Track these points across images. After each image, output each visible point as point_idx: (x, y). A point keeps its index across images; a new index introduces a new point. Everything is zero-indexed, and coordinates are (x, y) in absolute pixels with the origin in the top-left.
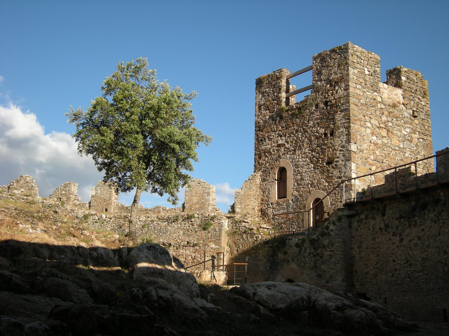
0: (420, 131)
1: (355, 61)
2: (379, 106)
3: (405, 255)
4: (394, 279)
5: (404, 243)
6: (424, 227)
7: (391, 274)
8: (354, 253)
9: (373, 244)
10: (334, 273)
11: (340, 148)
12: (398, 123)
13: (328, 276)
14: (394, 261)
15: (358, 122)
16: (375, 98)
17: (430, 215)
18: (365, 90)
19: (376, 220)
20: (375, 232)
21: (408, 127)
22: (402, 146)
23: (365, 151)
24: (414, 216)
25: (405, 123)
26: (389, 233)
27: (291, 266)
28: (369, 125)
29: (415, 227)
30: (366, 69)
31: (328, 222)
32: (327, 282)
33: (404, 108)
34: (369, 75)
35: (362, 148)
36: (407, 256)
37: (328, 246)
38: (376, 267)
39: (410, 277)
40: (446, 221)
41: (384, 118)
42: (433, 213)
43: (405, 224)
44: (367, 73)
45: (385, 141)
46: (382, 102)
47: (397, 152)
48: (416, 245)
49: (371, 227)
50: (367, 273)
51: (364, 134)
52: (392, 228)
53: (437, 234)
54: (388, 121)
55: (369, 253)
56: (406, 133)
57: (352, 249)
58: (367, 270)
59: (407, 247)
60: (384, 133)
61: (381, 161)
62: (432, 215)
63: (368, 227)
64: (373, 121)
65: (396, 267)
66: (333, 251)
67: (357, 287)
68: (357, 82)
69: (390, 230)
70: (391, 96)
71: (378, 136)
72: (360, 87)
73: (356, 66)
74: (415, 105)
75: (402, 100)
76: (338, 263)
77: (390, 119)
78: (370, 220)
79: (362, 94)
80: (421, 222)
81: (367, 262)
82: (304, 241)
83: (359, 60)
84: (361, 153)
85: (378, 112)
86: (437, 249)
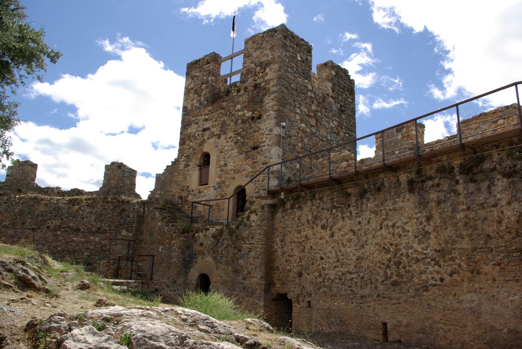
0: (346, 126)
1: (288, 44)
2: (309, 94)
3: (336, 252)
4: (321, 280)
5: (335, 238)
6: (360, 219)
7: (318, 274)
8: (276, 247)
9: (297, 238)
10: (252, 269)
11: (267, 132)
12: (327, 114)
13: (246, 272)
14: (322, 258)
15: (288, 106)
16: (306, 85)
17: (369, 205)
18: (296, 75)
19: (302, 211)
20: (300, 225)
21: (336, 121)
22: (329, 138)
23: (293, 138)
24: (349, 206)
25: (333, 116)
26: (317, 225)
27: (207, 259)
28: (298, 111)
29: (350, 219)
30: (298, 55)
31: (249, 211)
32: (244, 279)
33: (333, 101)
34: (301, 61)
35: (290, 133)
36: (338, 253)
37: (248, 238)
38: (300, 264)
39: (340, 279)
40: (390, 213)
41: (314, 107)
42: (373, 202)
43: (337, 216)
44: (299, 59)
45: (314, 130)
46: (311, 91)
47: (324, 143)
48: (350, 240)
49: (296, 219)
50: (290, 271)
51: (293, 119)
52: (321, 219)
53: (378, 228)
54: (317, 111)
55: (292, 247)
56: (334, 126)
57: (274, 242)
58: (289, 268)
59: (338, 243)
60: (313, 122)
61: (309, 150)
62: (372, 205)
63: (293, 218)
64: (302, 108)
65: (324, 266)
66: (253, 244)
67: (278, 286)
68: (289, 65)
69: (318, 222)
70: (321, 87)
71: (306, 123)
72: (292, 71)
73: (288, 49)
74: (343, 100)
75: (331, 93)
76: (258, 258)
77: (319, 109)
78: (296, 210)
79: (293, 78)
80: (357, 213)
81: (290, 258)
82: (221, 232)
83: (292, 44)
84: (289, 139)
85: (308, 100)
86: (377, 247)
